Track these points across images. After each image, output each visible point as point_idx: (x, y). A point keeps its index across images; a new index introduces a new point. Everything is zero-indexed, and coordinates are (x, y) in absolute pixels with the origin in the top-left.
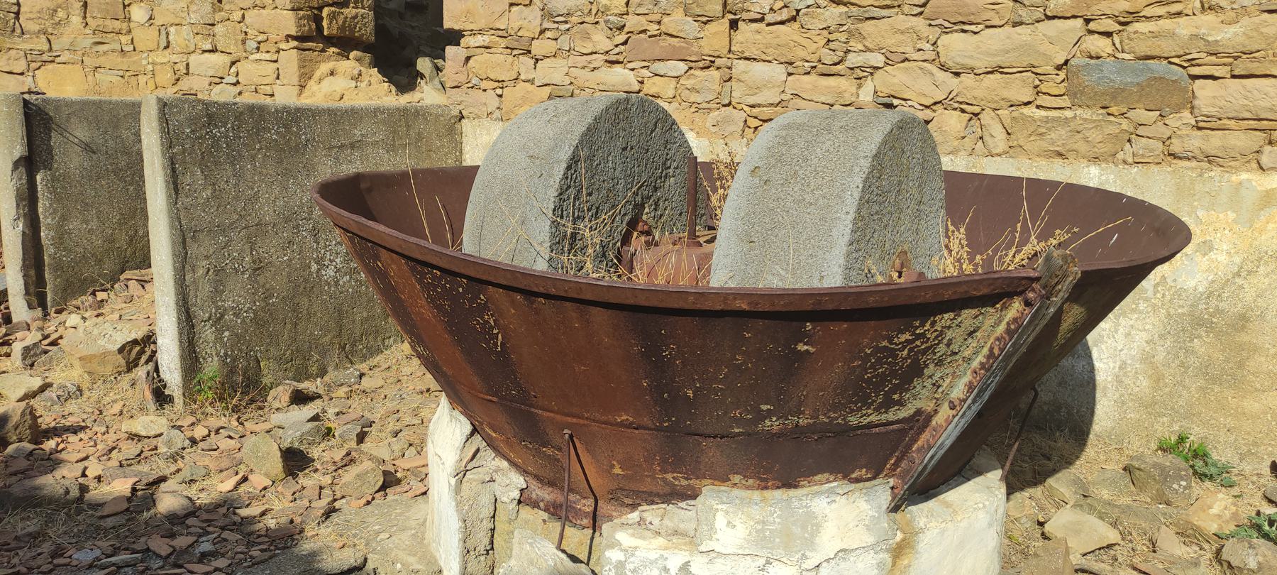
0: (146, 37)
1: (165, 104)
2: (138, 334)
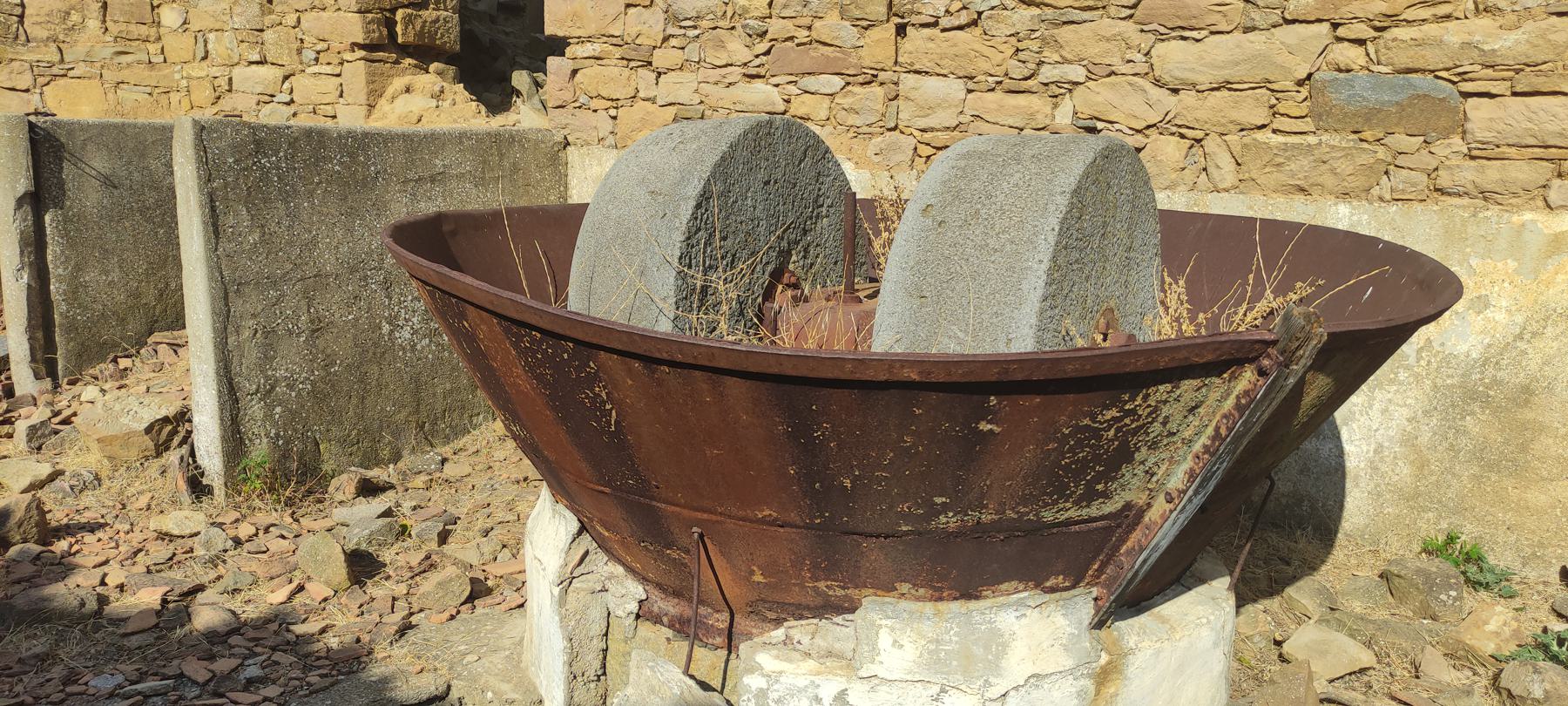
0: (179, 46)
1: (203, 128)
2: (170, 410)
